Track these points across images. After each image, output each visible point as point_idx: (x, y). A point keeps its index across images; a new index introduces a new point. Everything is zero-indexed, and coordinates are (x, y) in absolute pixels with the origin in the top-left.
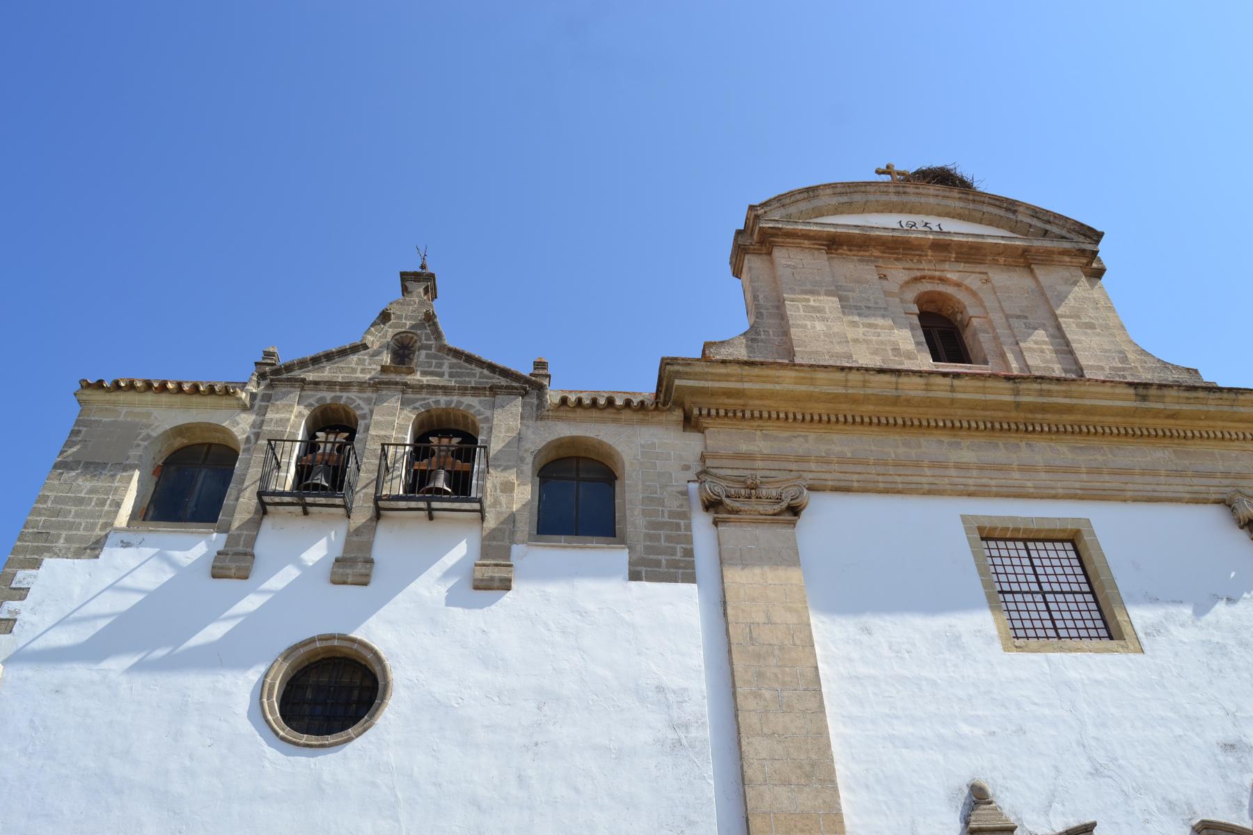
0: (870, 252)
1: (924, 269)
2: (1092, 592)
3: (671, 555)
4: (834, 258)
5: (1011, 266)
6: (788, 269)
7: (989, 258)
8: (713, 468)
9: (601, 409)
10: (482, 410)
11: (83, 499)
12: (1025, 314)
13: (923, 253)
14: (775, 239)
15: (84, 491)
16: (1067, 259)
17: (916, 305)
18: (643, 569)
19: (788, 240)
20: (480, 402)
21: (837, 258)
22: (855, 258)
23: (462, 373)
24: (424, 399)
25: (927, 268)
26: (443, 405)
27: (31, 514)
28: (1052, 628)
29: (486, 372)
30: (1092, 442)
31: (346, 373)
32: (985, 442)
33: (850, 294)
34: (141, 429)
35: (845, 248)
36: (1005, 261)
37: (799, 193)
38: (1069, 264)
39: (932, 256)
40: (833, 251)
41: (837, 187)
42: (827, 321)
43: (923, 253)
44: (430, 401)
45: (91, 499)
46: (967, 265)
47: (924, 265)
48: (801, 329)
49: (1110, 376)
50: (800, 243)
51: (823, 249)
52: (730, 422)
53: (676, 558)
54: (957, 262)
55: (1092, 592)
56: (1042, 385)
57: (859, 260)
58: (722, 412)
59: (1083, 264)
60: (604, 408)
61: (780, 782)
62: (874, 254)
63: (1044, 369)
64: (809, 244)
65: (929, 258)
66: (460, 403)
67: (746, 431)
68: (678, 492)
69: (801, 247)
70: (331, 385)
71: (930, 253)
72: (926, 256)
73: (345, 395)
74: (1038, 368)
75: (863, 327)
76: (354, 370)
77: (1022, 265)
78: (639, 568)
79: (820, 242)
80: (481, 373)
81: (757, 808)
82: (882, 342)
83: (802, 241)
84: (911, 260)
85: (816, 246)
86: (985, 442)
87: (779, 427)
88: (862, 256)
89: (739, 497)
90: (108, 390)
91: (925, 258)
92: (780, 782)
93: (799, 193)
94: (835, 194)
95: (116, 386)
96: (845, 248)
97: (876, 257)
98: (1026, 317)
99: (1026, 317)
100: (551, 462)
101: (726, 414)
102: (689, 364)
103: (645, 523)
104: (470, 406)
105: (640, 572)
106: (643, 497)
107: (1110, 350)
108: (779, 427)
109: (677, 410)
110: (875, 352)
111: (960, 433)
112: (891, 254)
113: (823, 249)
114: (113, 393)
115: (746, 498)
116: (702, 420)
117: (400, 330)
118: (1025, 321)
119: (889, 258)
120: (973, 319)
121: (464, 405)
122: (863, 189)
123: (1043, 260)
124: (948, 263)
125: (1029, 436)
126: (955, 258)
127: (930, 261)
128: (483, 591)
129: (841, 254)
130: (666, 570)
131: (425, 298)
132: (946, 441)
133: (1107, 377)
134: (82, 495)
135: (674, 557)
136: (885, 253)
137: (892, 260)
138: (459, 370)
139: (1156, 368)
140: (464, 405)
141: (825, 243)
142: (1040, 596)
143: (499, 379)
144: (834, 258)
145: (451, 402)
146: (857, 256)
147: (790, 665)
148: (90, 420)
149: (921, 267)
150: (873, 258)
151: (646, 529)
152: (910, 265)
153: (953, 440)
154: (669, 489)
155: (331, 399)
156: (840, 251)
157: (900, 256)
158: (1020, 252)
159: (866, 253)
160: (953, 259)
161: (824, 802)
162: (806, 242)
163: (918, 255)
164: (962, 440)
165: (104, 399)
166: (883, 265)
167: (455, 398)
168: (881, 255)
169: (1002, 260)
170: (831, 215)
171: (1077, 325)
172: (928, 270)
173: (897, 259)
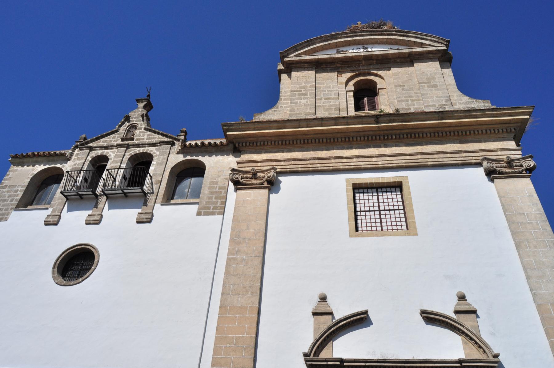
1: (360, 70)
2: (404, 209)
3: (216, 204)
5: (404, 62)
7: (392, 60)
8: (276, 166)
9: (199, 147)
10: (156, 152)
11: (6, 199)
13: (360, 63)
14: (292, 65)
15: (7, 197)
17: (353, 87)
18: (203, 211)
19: (298, 65)
20: (156, 149)
23: (151, 138)
24: (135, 150)
25: (361, 69)
26: (141, 152)
28: (393, 222)
29: (160, 136)
30: (417, 141)
31: (108, 142)
34: (31, 171)
35: (324, 65)
36: (400, 61)
37: (304, 43)
39: (364, 63)
41: (323, 38)
43: (360, 63)
44: (137, 150)
45: (8, 199)
46: (381, 65)
47: (361, 68)
48: (294, 104)
51: (313, 67)
52: (251, 148)
54: (377, 64)
55: (404, 209)
56: (391, 117)
58: (248, 144)
59: (439, 56)
60: (208, 147)
61: (235, 294)
64: (308, 66)
65: (363, 64)
66: (148, 150)
67: (258, 150)
69: (304, 67)
70: (101, 148)
71: (363, 62)
72: (362, 63)
73: (106, 151)
76: (111, 141)
78: (201, 211)
79: (312, 64)
80: (159, 137)
81: (223, 304)
82: (331, 106)
83: (304, 65)
84: (355, 66)
88: (332, 67)
89: (248, 179)
90: (19, 158)
91: (361, 64)
92: (235, 294)
93: (304, 43)
95: (24, 157)
97: (338, 67)
100: (182, 171)
101: (250, 144)
102: (232, 125)
103: (208, 192)
104: (151, 151)
105: (201, 212)
106: (210, 182)
109: (231, 144)
110: (326, 110)
112: (345, 65)
113: (313, 67)
114: (22, 159)
115: (251, 179)
116: (240, 148)
120: (379, 90)
121: (153, 152)
122: (335, 37)
123: (419, 58)
125: (386, 141)
126: (376, 62)
128: (498, 179)
132: (346, 147)
133: (436, 110)
134: (6, 198)
135: (216, 205)
136: (343, 65)
137: (346, 67)
138: (150, 137)
140: (153, 152)
141: (314, 64)
142: (381, 209)
143: (165, 139)
145: (144, 150)
148: (14, 170)
149: (359, 69)
150: (337, 68)
152: (355, 68)
155: (101, 153)
156: (322, 67)
157: (350, 65)
158: (407, 55)
161: (252, 301)
162: (306, 65)
163: (358, 64)
164: (353, 146)
165: (18, 161)
167: (146, 148)
168: (340, 66)
169: (399, 60)
170: (321, 51)
172: (362, 70)
173: (348, 67)
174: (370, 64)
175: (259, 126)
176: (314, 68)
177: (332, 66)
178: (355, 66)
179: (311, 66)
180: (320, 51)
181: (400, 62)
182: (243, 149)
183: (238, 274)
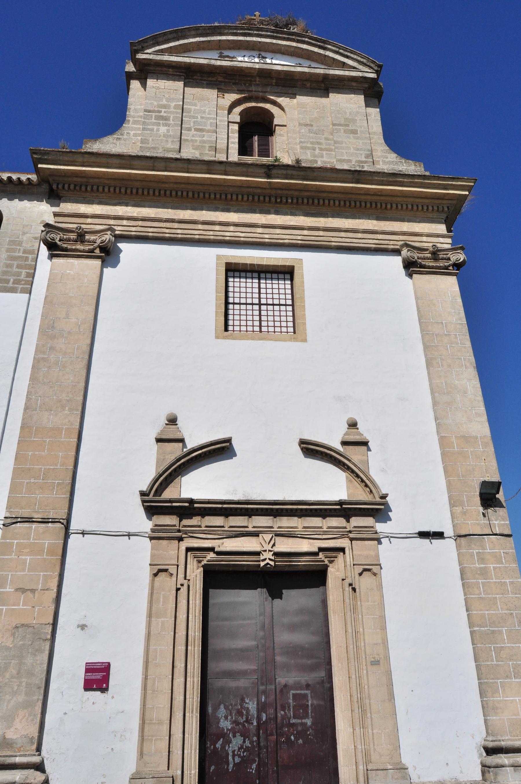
0: (216, 78)
1: (252, 91)
2: (293, 305)
4: (190, 82)
6: (154, 89)
12: (312, 124)
13: (253, 79)
14: (149, 68)
16: (354, 84)
19: (157, 69)
21: (192, 82)
22: (205, 82)
27: (457, 273)
30: (321, 210)
32: (247, 209)
33: (193, 108)
35: (198, 75)
36: (311, 85)
38: (355, 88)
40: (190, 77)
41: (199, 29)
42: (169, 126)
47: (253, 88)
49: (353, 166)
50: (166, 71)
53: (21, 278)
55: (293, 305)
57: (207, 84)
60: (6, 184)
61: (45, 410)
62: (219, 79)
63: (311, 161)
64: (173, 72)
65: (257, 83)
68: (33, 238)
69: (167, 74)
71: (258, 79)
72: (255, 81)
74: (307, 161)
75: (194, 131)
77: (323, 88)
82: (204, 142)
83: (168, 70)
84: (244, 84)
85: (178, 73)
86: (247, 209)
87: (110, 197)
88: (211, 81)
89: (70, 241)
91: (254, 83)
94: (197, 34)
96: (198, 75)
98: (312, 125)
99: (312, 125)
101: (75, 187)
103: (6, 257)
107: (361, 149)
108: (110, 197)
109: (45, 185)
110: (196, 148)
111: (231, 203)
115: (74, 241)
117: (329, 153)
118: (310, 128)
119: (230, 83)
120: (277, 127)
124: (270, 87)
125: (278, 205)
126: (276, 83)
127: (258, 85)
129: (196, 79)
130: (12, 285)
131: (298, 129)
133: (352, 167)
135: (19, 278)
136: (226, 79)
139: (393, 162)
141: (183, 71)
144: (190, 82)
146: (207, 81)
147: (73, 343)
151: (6, 260)
152: (243, 87)
153: (226, 207)
154: (28, 235)
156: (195, 77)
159: (213, 79)
160: (274, 84)
162: (170, 70)
166: (223, 88)
169: (308, 85)
170: (196, 50)
171: (345, 131)
172: (255, 91)
173: (235, 84)
174: (267, 85)
175: (92, 161)
176: (183, 77)
177: (210, 79)
178: (245, 84)
179: (178, 73)
180: (193, 50)
181: (311, 88)
182: (63, 193)
183: (50, 382)
